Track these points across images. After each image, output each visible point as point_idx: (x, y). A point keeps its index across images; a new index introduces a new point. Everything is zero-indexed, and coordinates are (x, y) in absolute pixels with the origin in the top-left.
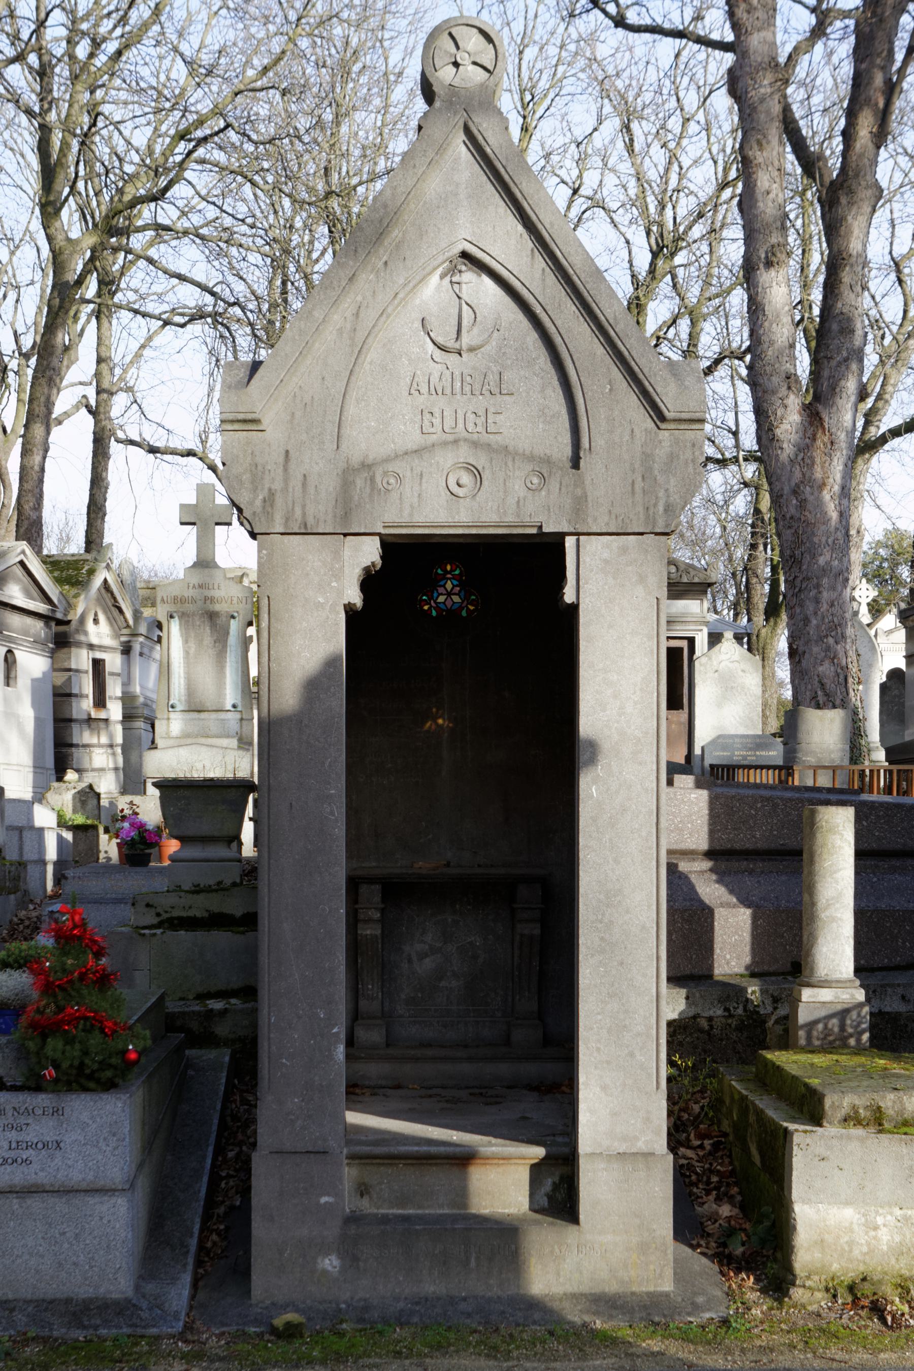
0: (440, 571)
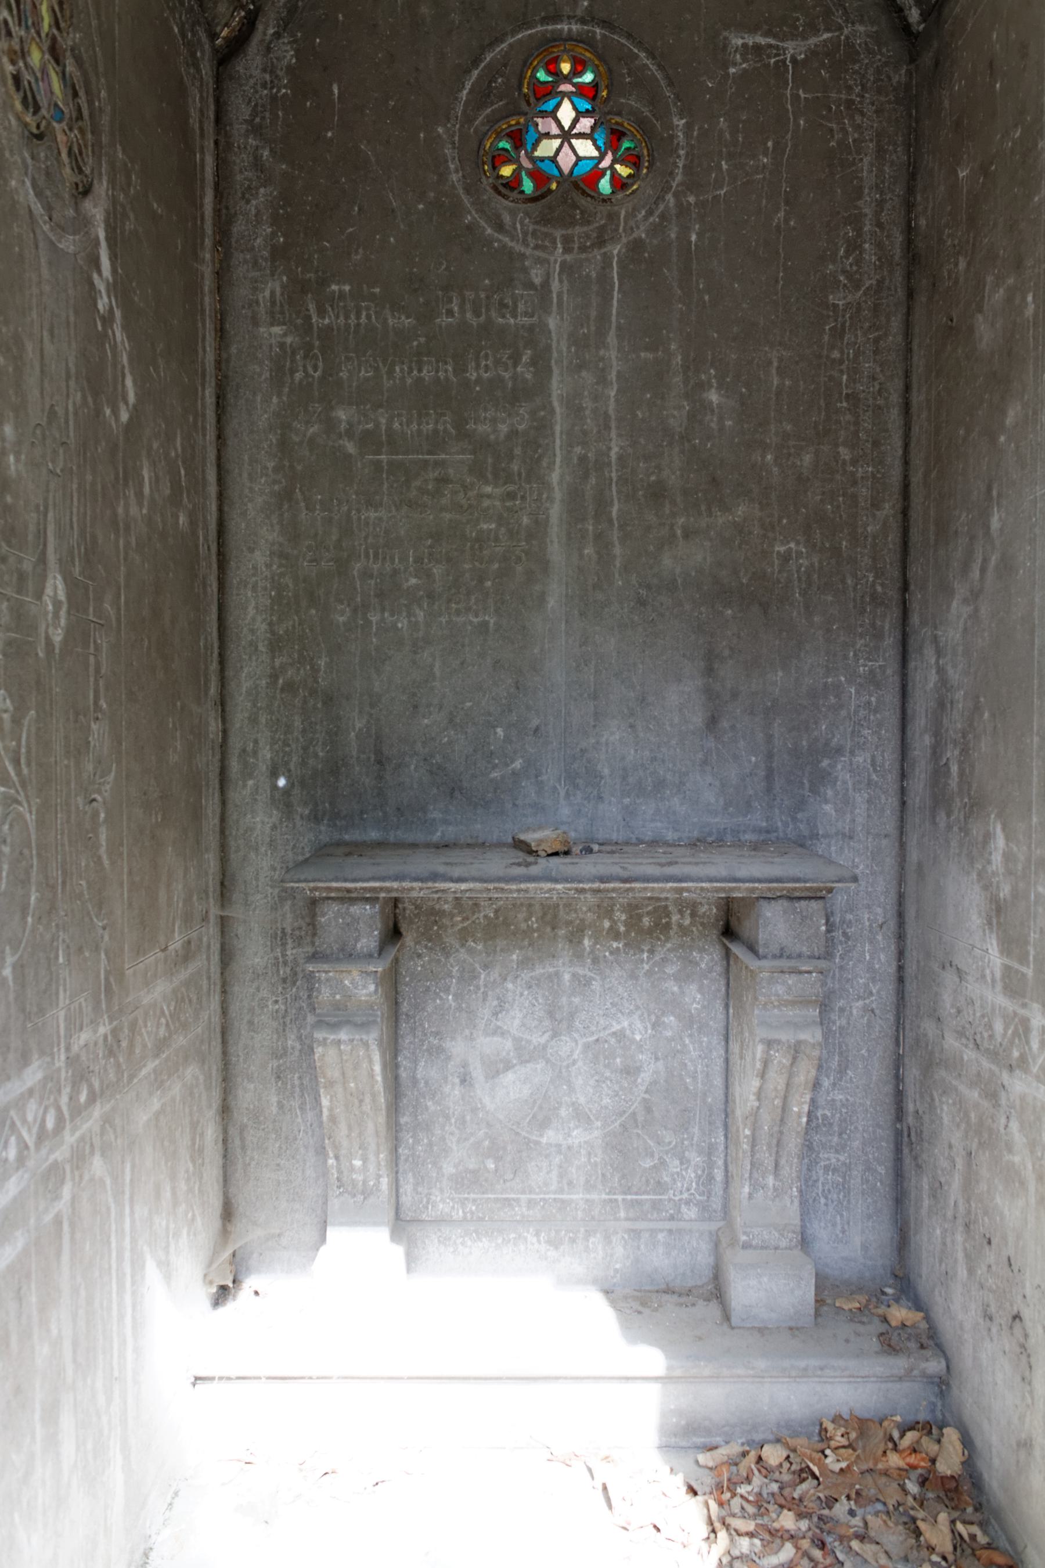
0: (542, 76)
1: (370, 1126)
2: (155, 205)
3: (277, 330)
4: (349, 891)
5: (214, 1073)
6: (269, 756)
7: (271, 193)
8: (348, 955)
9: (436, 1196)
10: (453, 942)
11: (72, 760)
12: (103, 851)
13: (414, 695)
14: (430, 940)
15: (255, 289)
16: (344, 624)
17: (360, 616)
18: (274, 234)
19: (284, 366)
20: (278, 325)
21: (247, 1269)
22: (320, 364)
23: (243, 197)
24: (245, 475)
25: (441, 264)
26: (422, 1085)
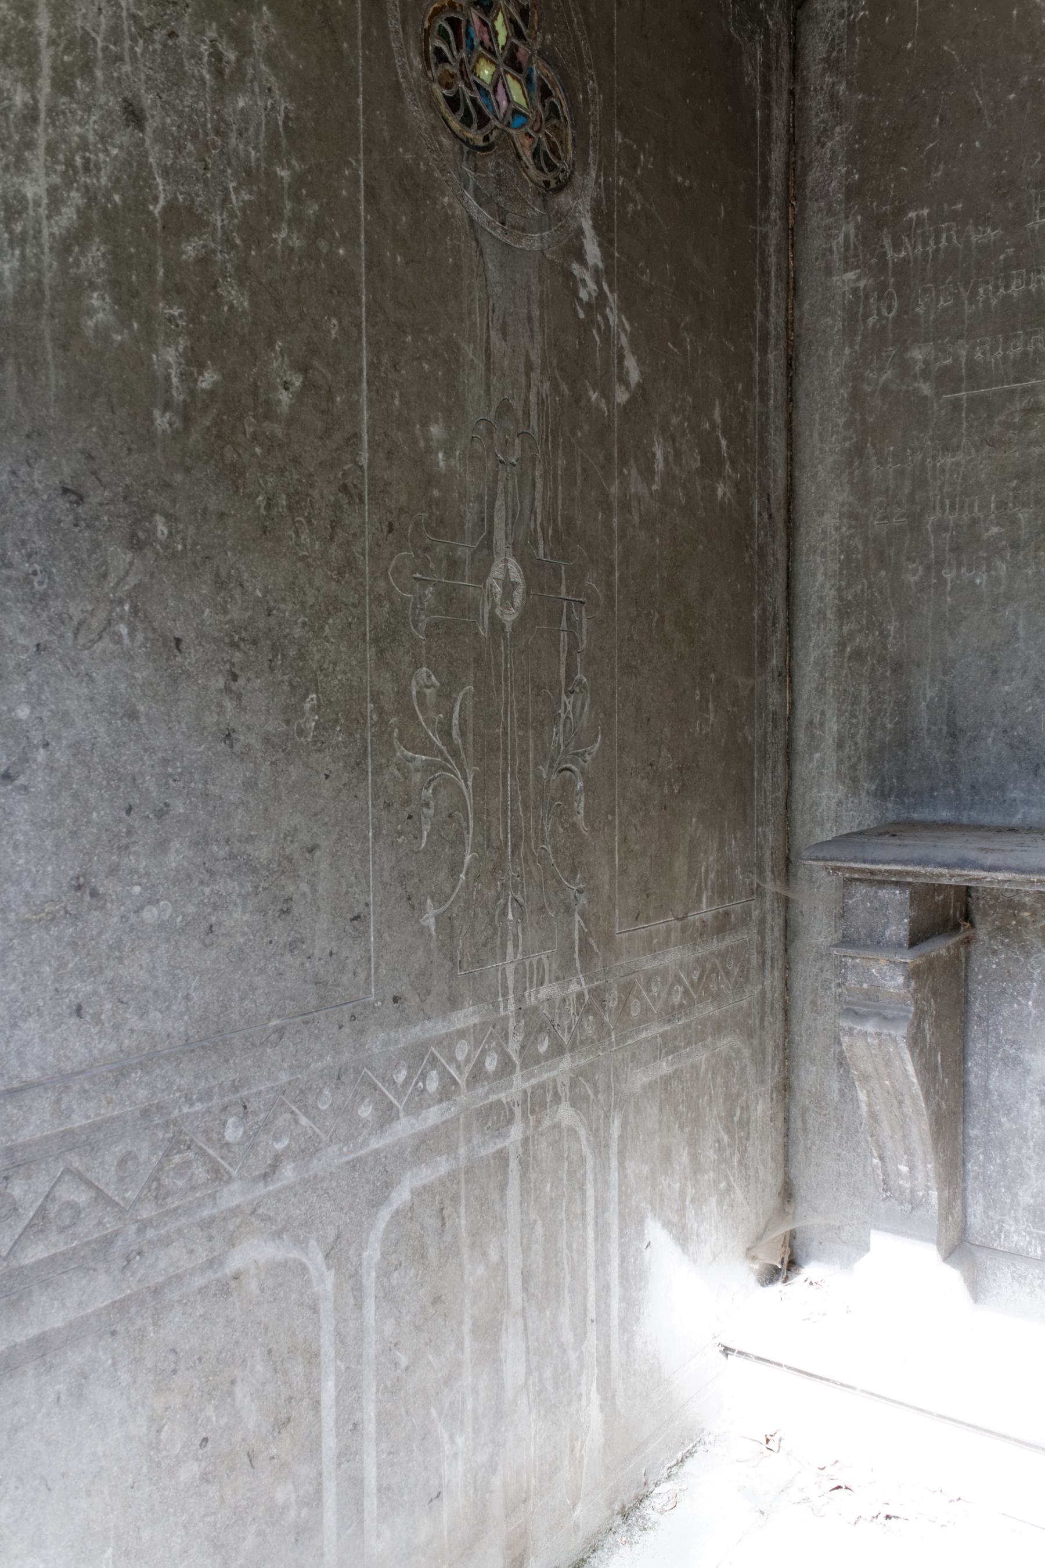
1: (914, 1130)
2: (680, 179)
3: (851, 275)
4: (872, 872)
5: (770, 1048)
6: (835, 728)
7: (847, 128)
8: (876, 943)
9: (1010, 1226)
10: (1034, 940)
11: (531, 733)
12: (580, 818)
13: (993, 658)
14: (1007, 936)
15: (829, 237)
16: (916, 584)
17: (933, 574)
18: (849, 173)
19: (857, 313)
20: (852, 269)
21: (807, 1255)
22: (896, 304)
23: (819, 142)
24: (816, 436)
25: (1035, 157)
26: (995, 1097)
